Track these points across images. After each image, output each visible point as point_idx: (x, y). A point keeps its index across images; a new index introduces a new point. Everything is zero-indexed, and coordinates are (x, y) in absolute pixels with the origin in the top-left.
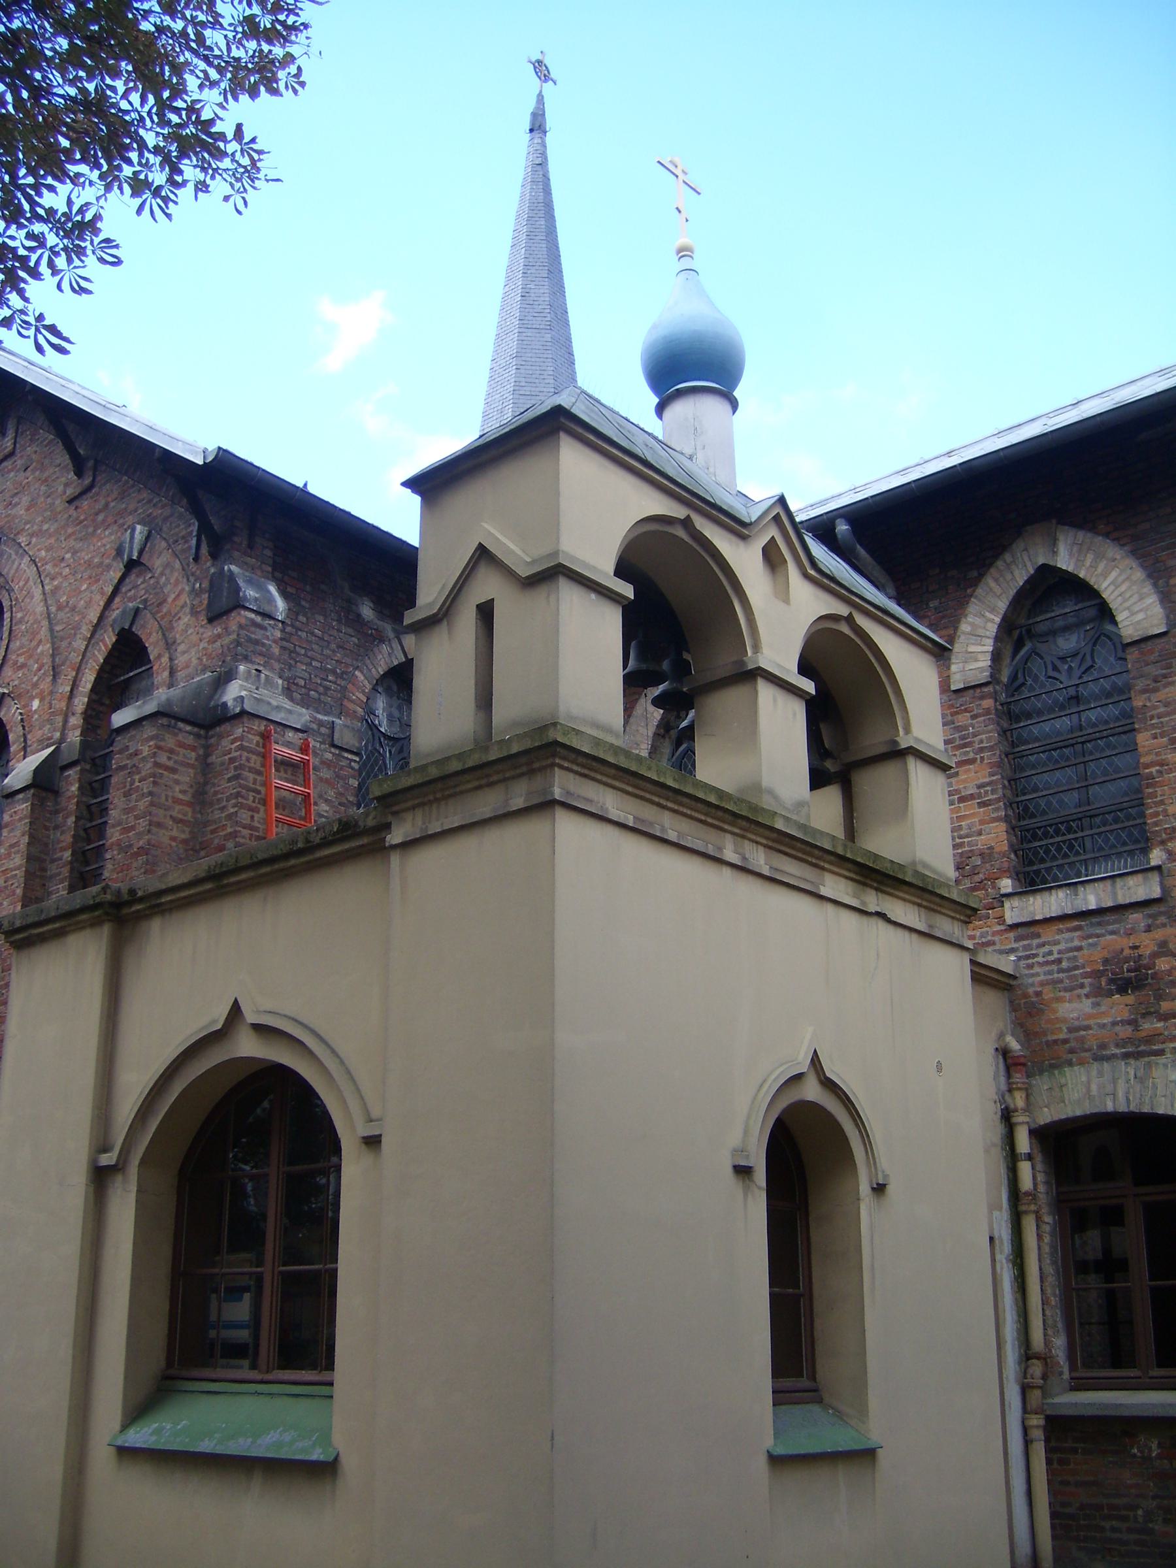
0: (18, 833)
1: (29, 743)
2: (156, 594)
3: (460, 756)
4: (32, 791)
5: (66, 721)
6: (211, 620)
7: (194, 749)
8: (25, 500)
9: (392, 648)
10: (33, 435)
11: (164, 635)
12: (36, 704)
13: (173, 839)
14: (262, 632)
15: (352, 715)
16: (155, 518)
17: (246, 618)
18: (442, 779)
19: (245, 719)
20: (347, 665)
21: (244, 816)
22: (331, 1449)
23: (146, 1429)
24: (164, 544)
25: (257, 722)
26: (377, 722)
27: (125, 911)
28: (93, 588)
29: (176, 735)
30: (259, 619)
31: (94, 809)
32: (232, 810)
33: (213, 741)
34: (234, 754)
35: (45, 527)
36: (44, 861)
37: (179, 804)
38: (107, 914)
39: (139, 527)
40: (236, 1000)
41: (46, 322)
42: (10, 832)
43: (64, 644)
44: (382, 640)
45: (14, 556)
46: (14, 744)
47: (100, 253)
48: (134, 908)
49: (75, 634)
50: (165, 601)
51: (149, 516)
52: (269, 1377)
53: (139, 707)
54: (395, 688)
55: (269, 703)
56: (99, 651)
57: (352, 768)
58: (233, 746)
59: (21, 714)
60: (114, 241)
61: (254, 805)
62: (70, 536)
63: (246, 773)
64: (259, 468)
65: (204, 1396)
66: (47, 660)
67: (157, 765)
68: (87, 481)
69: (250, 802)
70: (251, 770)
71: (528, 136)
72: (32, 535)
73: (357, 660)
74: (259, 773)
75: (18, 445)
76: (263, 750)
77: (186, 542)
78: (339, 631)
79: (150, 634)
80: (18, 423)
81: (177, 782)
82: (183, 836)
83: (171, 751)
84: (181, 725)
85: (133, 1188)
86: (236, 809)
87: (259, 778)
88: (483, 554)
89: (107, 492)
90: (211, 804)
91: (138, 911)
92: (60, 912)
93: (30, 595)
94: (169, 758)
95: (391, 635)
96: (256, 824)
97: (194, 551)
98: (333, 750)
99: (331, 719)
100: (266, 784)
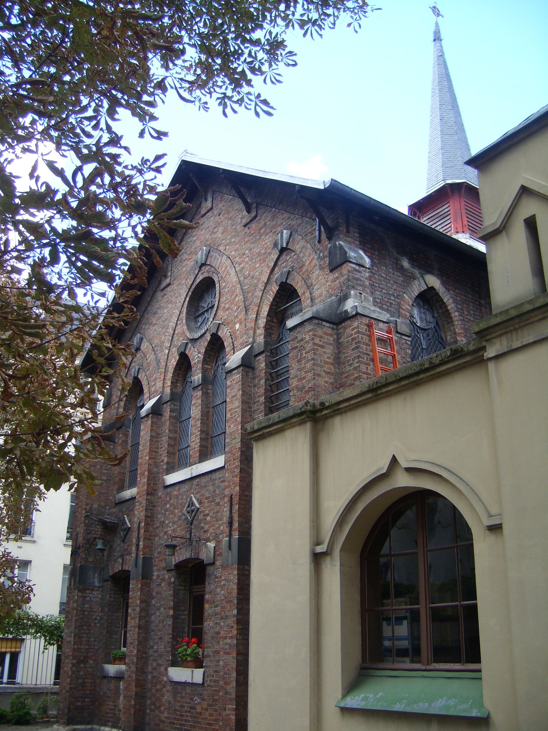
0: (236, 390)
1: (235, 346)
2: (298, 263)
3: (530, 302)
4: (241, 368)
5: (255, 332)
6: (331, 271)
7: (332, 335)
8: (221, 229)
9: (419, 282)
10: (221, 198)
11: (305, 282)
12: (237, 326)
13: (326, 382)
14: (360, 274)
15: (405, 317)
16: (293, 226)
17: (351, 267)
18: (519, 316)
19: (359, 317)
20: (399, 291)
21: (363, 367)
22: (483, 710)
23: (357, 698)
24: (300, 237)
25: (364, 318)
26: (415, 321)
27: (318, 415)
28: (263, 265)
29: (323, 328)
30: (357, 267)
31: (273, 375)
32: (356, 365)
33: (341, 331)
34: (354, 336)
35: (233, 240)
36: (250, 403)
37: (327, 364)
38: (308, 417)
39: (285, 231)
40: (394, 456)
41: (261, 98)
42: (231, 390)
43: (250, 295)
44: (414, 278)
45: (218, 257)
46: (227, 347)
47: (285, 60)
48: (324, 413)
49: (255, 289)
50: (304, 265)
51: (289, 225)
52: (428, 667)
53: (302, 316)
54: (421, 304)
55: (369, 309)
56: (270, 295)
57: (408, 344)
58: (353, 332)
59: (230, 332)
60: (293, 52)
61: (367, 362)
62: (247, 242)
63: (362, 345)
64: (352, 189)
65: (390, 678)
66: (242, 304)
67: (314, 344)
68: (253, 214)
69: (365, 360)
70: (364, 343)
71: (433, 43)
72: (226, 245)
73: (403, 289)
74: (368, 345)
75: (214, 204)
76: (368, 333)
77: (312, 234)
78: (393, 274)
79: (298, 283)
80: (213, 194)
81: (325, 353)
82: (331, 381)
83: (321, 337)
84: (324, 323)
85: (338, 563)
86: (359, 364)
87: (368, 348)
88: (524, 191)
89: (265, 218)
90: (344, 363)
91: (326, 414)
92: (281, 418)
93: (229, 274)
94: (320, 341)
95: (419, 276)
96: (369, 371)
97: (318, 238)
98: (397, 335)
99: (395, 319)
100: (373, 351)
